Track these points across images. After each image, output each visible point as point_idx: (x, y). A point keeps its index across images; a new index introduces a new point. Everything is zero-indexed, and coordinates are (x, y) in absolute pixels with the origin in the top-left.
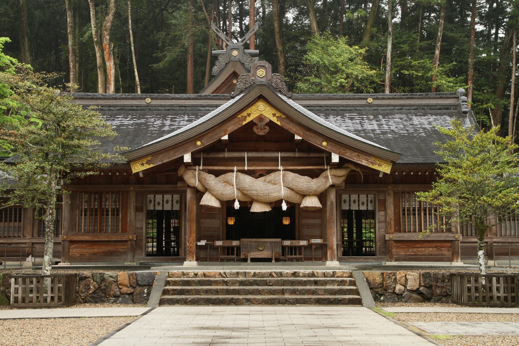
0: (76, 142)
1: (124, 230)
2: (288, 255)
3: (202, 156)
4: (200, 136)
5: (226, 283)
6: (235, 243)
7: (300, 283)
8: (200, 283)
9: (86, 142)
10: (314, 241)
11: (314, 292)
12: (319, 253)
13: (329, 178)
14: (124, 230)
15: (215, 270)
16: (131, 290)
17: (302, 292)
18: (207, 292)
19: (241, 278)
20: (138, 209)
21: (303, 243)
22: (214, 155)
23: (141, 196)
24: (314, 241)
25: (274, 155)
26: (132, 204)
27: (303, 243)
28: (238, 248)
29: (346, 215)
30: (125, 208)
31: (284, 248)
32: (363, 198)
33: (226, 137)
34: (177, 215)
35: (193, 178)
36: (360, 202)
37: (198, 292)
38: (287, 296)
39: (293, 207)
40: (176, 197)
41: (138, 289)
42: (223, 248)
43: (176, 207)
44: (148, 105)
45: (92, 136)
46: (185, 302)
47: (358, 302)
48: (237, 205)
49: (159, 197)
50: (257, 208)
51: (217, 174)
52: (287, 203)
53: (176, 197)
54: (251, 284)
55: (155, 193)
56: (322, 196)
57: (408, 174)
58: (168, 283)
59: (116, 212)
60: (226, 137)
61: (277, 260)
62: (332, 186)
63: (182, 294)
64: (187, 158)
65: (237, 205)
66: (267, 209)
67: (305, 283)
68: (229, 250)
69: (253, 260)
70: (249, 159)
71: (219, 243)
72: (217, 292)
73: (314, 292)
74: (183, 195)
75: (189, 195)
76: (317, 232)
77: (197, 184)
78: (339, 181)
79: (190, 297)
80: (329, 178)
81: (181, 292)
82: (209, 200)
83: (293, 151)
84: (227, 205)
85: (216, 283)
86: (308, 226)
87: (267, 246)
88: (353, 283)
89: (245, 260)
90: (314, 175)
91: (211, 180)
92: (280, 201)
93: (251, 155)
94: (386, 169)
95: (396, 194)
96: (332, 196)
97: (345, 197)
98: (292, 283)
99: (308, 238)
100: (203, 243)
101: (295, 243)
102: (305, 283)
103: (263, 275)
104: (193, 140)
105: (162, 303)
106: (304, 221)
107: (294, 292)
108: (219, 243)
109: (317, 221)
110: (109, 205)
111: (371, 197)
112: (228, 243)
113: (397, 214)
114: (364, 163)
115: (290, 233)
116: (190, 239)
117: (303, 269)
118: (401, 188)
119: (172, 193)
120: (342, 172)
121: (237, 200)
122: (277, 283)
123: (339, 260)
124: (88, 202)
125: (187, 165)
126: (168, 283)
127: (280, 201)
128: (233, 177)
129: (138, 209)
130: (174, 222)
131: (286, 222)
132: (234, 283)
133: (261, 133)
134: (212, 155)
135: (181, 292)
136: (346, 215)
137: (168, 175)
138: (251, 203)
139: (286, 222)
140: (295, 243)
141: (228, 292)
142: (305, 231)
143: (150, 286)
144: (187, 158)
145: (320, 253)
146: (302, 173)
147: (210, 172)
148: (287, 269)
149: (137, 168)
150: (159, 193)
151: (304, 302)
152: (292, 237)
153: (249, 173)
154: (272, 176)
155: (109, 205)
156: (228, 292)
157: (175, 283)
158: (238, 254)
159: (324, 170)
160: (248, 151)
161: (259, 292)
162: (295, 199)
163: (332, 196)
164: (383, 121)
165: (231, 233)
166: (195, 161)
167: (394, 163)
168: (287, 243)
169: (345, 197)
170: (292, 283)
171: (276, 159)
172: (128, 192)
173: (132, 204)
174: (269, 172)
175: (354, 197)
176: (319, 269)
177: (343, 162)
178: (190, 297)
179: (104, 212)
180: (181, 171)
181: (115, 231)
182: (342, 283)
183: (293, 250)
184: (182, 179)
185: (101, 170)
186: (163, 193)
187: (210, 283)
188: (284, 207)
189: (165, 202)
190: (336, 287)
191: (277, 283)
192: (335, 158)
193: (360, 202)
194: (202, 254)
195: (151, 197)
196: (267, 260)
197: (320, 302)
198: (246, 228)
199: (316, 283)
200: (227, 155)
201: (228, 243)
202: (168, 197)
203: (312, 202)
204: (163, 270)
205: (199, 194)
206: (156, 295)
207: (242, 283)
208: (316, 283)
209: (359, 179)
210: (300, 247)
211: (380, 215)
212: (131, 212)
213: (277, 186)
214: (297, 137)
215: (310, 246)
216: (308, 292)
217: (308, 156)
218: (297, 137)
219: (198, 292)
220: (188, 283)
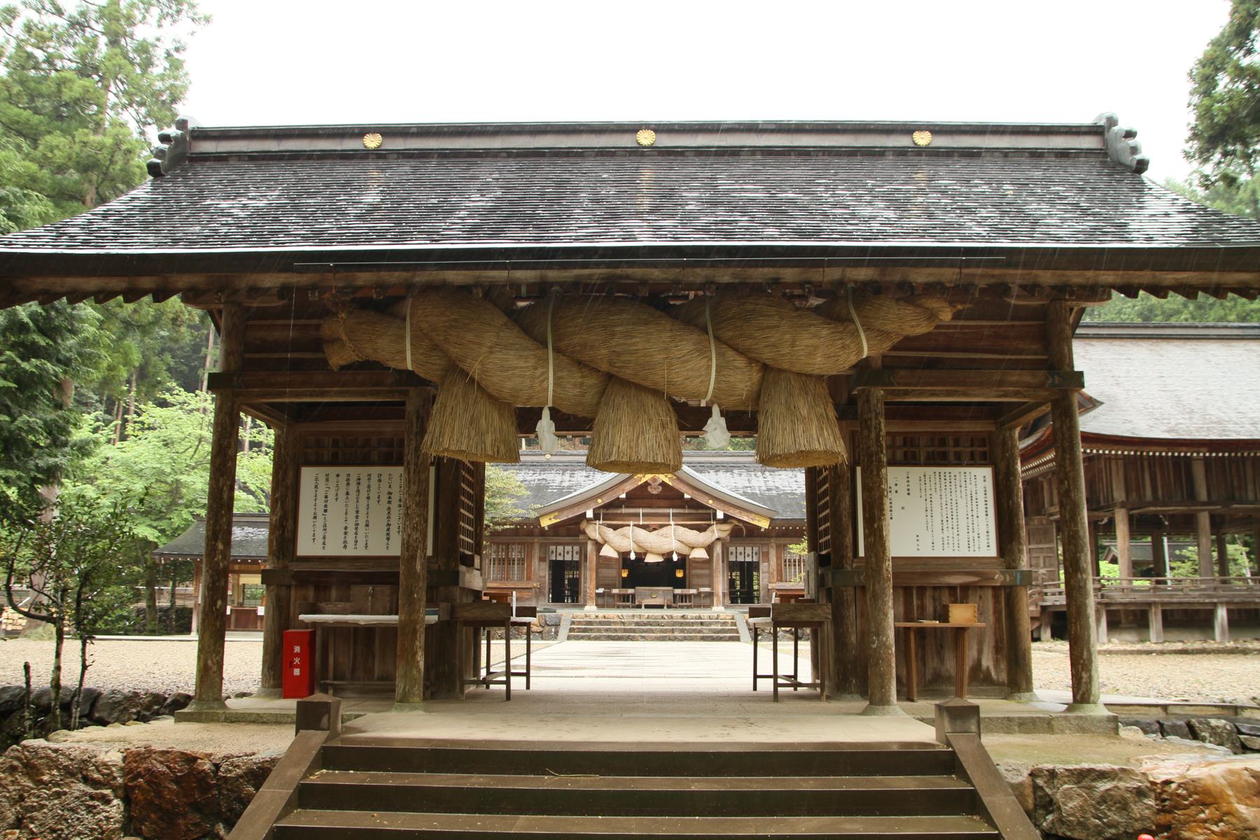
0: (497, 501)
1: (529, 579)
2: (677, 602)
3: (602, 512)
4: (600, 495)
5: (623, 623)
6: (630, 591)
7: (688, 624)
8: (601, 623)
9: (505, 501)
10: (702, 590)
11: (700, 632)
12: (707, 601)
13: (716, 532)
14: (529, 579)
15: (613, 614)
16: (540, 629)
17: (689, 631)
18: (607, 630)
19: (636, 620)
20: (542, 559)
21: (693, 591)
22: (611, 511)
23: (545, 547)
24: (702, 590)
25: (667, 511)
26: (536, 554)
27: (693, 591)
28: (633, 596)
29: (733, 566)
30: (530, 557)
31: (675, 596)
32: (749, 550)
33: (623, 496)
34: (575, 566)
35: (594, 531)
36: (745, 554)
37: (599, 630)
38: (676, 634)
39: (683, 559)
40: (576, 548)
41: (547, 628)
42: (619, 595)
43: (576, 558)
44: (548, 461)
45: (512, 496)
46: (589, 638)
47: (737, 639)
48: (633, 556)
49: (560, 549)
50: (650, 559)
51: (615, 528)
52: (679, 554)
53: (576, 548)
54: (645, 624)
55: (557, 544)
56: (709, 549)
57: (787, 529)
58: (573, 623)
59: (521, 561)
60: (623, 496)
61: (669, 607)
62: (718, 539)
63: (582, 632)
64: (590, 514)
65: (633, 556)
66: (660, 559)
67: (693, 624)
68: (625, 598)
69: (647, 607)
70: (644, 515)
71: (615, 591)
72: (616, 630)
73: (700, 632)
74: (583, 546)
75: (590, 547)
76: (706, 581)
77: (598, 537)
78: (724, 535)
79: (593, 634)
80: (716, 532)
81: (585, 630)
82: (607, 551)
83: (683, 507)
84: (624, 555)
85: (615, 623)
86: (698, 576)
87: (660, 594)
88: (734, 624)
89: (639, 607)
90: (701, 529)
91: (610, 533)
92: (671, 553)
93: (646, 511)
94: (764, 524)
95: (778, 547)
96: (718, 549)
97: (732, 549)
98: (681, 624)
99: (697, 587)
100: (601, 590)
101: (686, 591)
102: (693, 624)
103: (656, 618)
104: (594, 498)
105: (569, 638)
106: (694, 572)
107: (682, 631)
108: (615, 591)
109: (706, 572)
110: (515, 555)
111: (756, 549)
112: (624, 591)
113: (779, 565)
114: (745, 519)
115: (681, 583)
116: (589, 585)
117: (691, 614)
118: (782, 541)
119: (572, 544)
120: (727, 527)
121: (546, 414)
122: (668, 624)
123: (726, 607)
124: (497, 552)
125: (589, 520)
126: (573, 623)
127: (671, 553)
128: (628, 531)
129: (542, 559)
130: (568, 575)
131: (679, 574)
132: (630, 624)
133: (655, 492)
134: (611, 511)
135: (585, 630)
136: (733, 566)
137: (571, 529)
138: (645, 554)
139: (679, 574)
140: (686, 591)
141: (625, 631)
142: (695, 581)
143: (557, 625)
144: (590, 514)
145: (706, 600)
146: (691, 527)
147: (609, 526)
148: (677, 613)
149: (545, 523)
150: (560, 544)
151: (691, 639)
152: (683, 587)
153: (644, 527)
154: (665, 529)
155: (515, 555)
156: (625, 631)
157: (579, 623)
158: (633, 601)
159: (710, 525)
160: (643, 507)
161: (652, 631)
162: (685, 551)
163: (718, 549)
164: (769, 478)
165: (626, 583)
166: (596, 517)
167: (772, 520)
168: (678, 591)
169: (732, 549)
170: (681, 624)
171: (668, 515)
172: (532, 544)
173: (536, 554)
174: (662, 526)
175: (740, 549)
176: (704, 613)
177: (727, 519)
178: (593, 634)
179: (510, 562)
180: (583, 525)
181: (521, 579)
182: (725, 624)
183: (684, 598)
184: (584, 533)
185: (516, 524)
186: (564, 544)
187: (609, 623)
188: (675, 558)
189: (566, 553)
190: (719, 627)
191: (668, 624)
192: (720, 515)
193: (745, 554)
194: (600, 601)
195: (553, 548)
196: (661, 607)
197: (704, 639)
198: (640, 574)
199: (702, 624)
200: (624, 511)
201: (624, 591)
202: (568, 548)
203: (700, 554)
204: (566, 614)
205: (599, 546)
206: (564, 632)
207: (637, 624)
208: (702, 624)
209: (743, 533)
210: (690, 596)
211: (763, 566)
212: (536, 562)
213: (668, 539)
214: (686, 496)
215: (699, 594)
216: (694, 631)
217: (697, 512)
218: (686, 496)
219: (599, 630)
220: (590, 623)
